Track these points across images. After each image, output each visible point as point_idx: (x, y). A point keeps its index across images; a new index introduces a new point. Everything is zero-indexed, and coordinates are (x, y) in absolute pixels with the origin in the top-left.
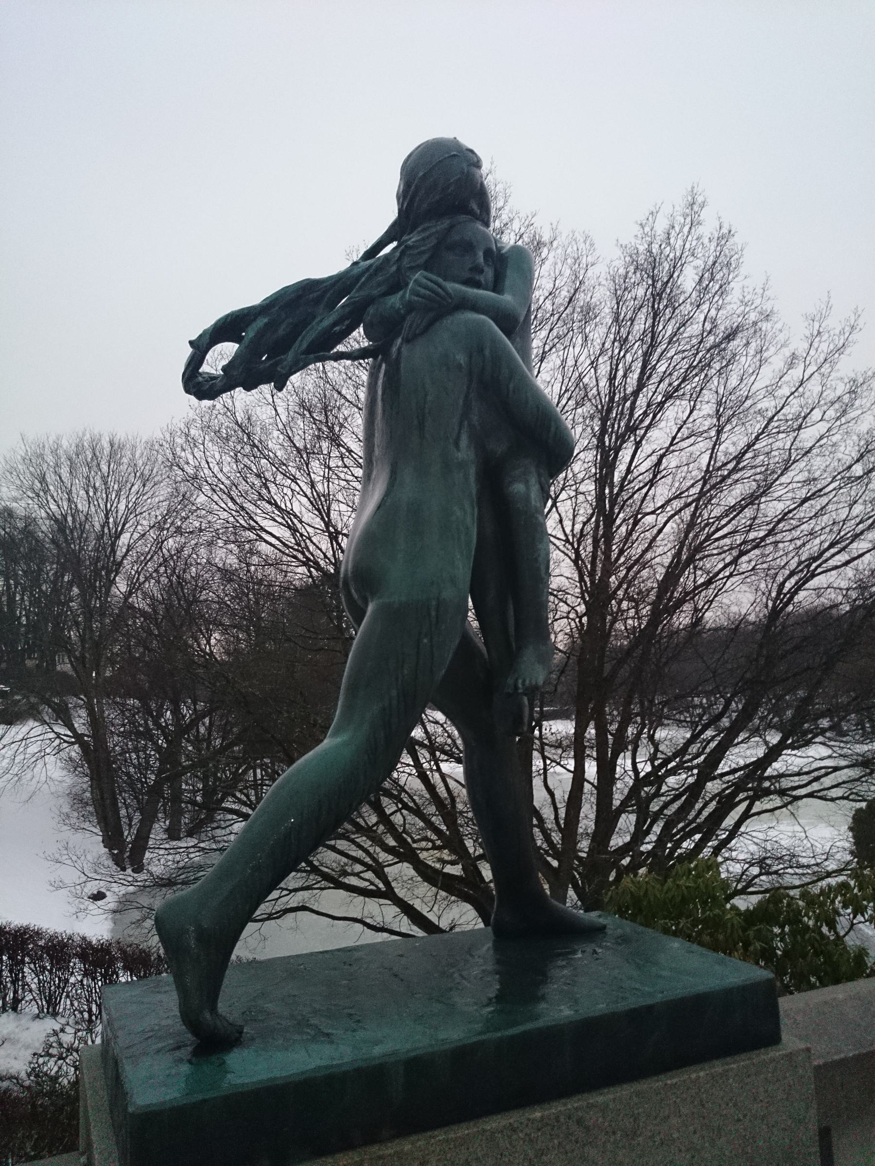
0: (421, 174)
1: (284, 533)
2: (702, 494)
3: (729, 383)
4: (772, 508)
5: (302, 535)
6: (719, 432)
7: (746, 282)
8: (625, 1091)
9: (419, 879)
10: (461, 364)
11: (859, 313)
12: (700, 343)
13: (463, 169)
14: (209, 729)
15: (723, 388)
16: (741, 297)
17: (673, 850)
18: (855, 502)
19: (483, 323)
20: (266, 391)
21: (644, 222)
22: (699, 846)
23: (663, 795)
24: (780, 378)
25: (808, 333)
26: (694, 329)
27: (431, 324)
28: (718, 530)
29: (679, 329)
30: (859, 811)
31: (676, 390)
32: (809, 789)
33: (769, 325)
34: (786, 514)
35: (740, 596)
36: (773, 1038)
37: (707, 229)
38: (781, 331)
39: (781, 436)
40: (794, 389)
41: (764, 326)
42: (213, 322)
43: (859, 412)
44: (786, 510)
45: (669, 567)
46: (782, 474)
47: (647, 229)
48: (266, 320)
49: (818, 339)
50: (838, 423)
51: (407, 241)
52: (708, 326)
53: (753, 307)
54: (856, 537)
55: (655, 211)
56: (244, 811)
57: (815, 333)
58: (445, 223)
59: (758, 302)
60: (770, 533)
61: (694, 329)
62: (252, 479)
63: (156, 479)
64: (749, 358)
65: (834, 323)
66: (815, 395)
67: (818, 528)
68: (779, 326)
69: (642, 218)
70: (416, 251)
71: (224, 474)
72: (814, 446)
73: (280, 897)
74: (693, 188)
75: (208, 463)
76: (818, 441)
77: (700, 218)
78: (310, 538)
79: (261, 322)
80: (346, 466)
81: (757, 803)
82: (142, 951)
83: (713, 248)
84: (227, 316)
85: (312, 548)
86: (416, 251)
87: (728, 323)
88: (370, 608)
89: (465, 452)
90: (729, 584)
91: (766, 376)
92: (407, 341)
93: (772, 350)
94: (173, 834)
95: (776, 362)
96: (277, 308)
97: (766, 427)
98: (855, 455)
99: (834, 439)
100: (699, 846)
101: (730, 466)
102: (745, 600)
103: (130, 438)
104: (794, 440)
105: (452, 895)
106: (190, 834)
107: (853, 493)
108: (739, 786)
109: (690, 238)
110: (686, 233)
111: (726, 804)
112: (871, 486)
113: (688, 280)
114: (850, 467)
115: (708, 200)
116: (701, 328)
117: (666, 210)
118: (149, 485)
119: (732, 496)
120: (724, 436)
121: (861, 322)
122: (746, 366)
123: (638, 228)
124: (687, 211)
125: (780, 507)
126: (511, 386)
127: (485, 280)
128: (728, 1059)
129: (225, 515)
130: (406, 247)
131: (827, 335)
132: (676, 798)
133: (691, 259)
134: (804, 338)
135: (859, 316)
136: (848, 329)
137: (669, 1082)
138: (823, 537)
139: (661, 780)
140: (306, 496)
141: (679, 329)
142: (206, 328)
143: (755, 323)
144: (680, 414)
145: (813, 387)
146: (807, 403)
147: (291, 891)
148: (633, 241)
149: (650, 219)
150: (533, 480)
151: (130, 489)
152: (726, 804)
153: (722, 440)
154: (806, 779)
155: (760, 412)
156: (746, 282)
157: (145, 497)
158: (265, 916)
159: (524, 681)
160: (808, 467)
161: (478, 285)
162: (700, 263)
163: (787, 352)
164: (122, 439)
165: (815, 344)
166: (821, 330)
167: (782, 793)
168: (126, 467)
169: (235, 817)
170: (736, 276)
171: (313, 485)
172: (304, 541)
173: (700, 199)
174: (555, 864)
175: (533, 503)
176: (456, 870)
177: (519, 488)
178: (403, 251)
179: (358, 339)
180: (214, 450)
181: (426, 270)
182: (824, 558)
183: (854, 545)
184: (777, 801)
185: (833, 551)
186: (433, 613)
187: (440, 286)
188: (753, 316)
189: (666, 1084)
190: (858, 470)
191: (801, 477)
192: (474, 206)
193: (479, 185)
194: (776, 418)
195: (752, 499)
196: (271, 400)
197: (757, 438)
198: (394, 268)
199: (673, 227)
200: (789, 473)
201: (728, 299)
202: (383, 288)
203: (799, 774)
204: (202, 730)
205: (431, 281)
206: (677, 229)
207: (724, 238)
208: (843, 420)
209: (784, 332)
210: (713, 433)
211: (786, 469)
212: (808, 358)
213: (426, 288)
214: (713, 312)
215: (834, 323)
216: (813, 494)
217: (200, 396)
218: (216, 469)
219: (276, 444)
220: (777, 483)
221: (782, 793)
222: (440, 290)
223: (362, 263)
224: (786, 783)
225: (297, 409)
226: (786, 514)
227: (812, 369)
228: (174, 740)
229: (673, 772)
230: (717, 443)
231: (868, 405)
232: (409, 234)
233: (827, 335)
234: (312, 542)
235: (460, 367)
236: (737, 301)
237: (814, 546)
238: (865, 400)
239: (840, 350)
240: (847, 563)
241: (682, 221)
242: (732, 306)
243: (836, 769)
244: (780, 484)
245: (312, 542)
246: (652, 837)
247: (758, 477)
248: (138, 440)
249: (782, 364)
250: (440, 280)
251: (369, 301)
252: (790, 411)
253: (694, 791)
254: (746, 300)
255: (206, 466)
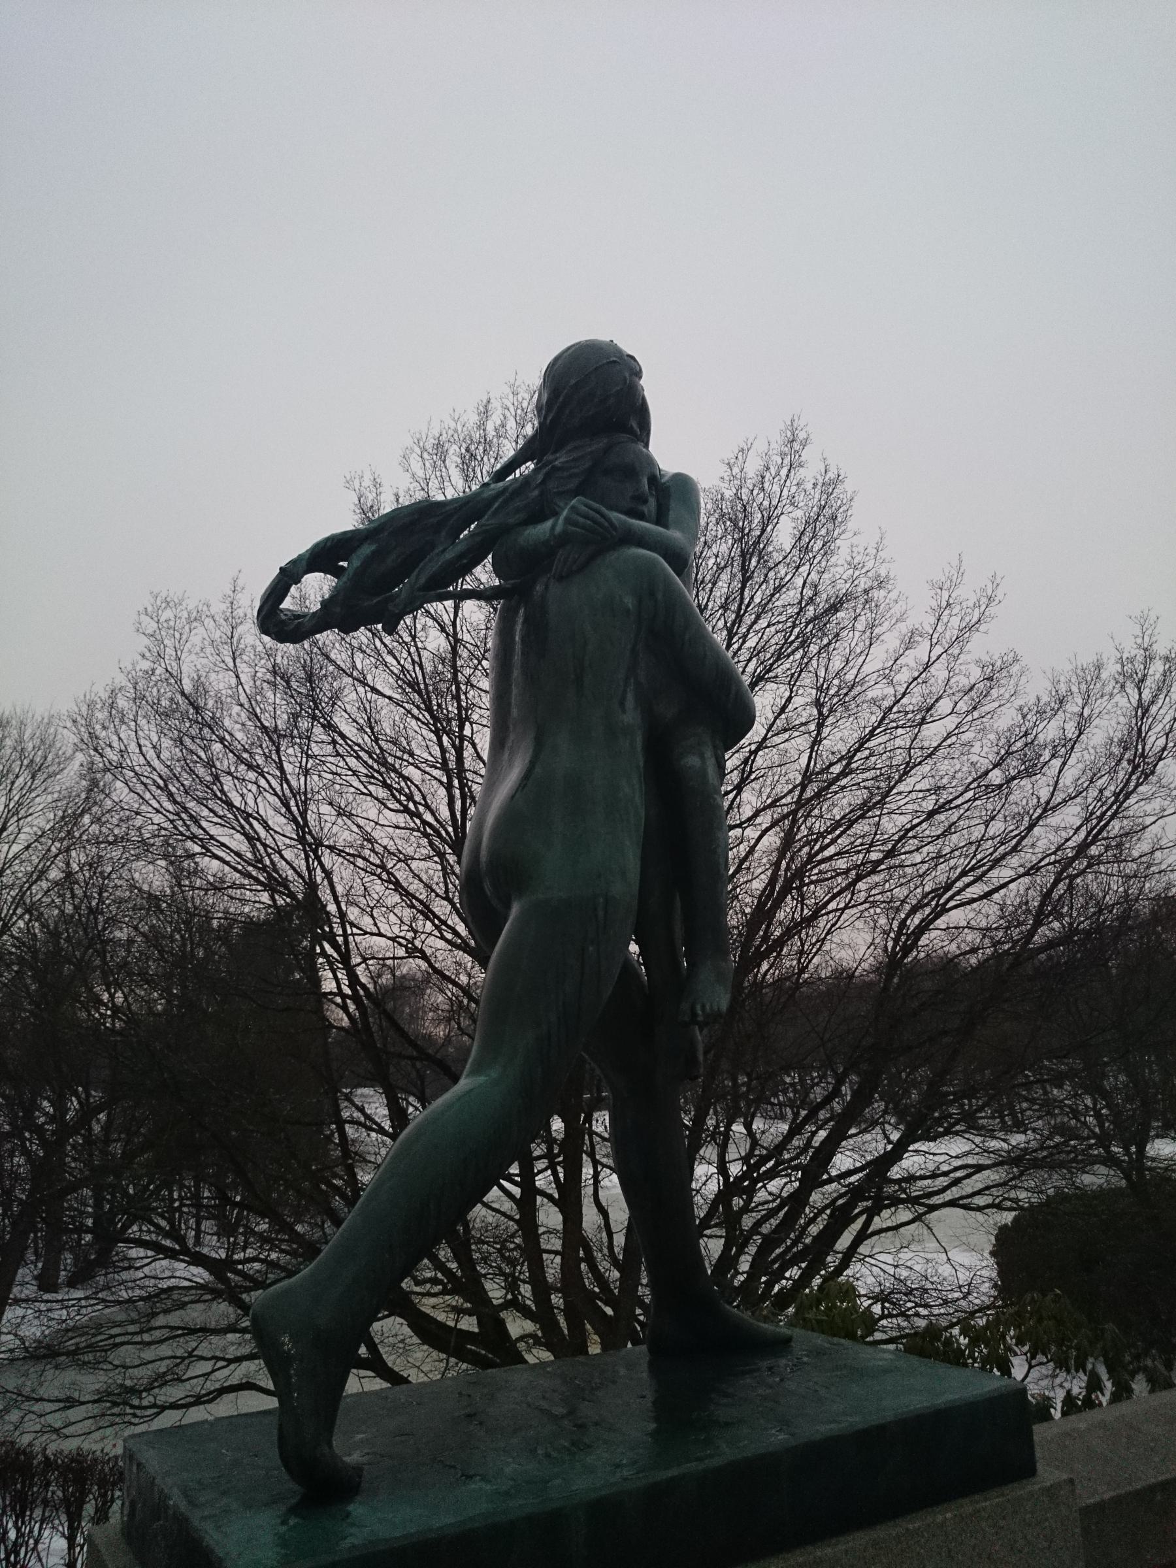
0: (573, 382)
1: (238, 842)
2: (800, 804)
3: (831, 665)
4: (891, 825)
5: (265, 846)
6: (820, 726)
7: (855, 540)
8: (859, 1540)
9: (416, 1340)
10: (629, 610)
11: (998, 581)
12: (798, 614)
13: (625, 377)
14: (107, 1128)
15: (823, 670)
16: (849, 559)
17: (770, 1285)
18: (993, 818)
19: (653, 564)
20: (225, 652)
21: (732, 461)
22: (806, 1278)
23: (752, 1211)
24: (896, 661)
25: (934, 604)
26: (790, 596)
27: (592, 558)
28: (822, 849)
29: (772, 595)
30: (1003, 1231)
31: (769, 671)
32: (948, 1196)
33: (883, 593)
34: (908, 831)
35: (854, 935)
36: (1029, 1470)
37: (809, 473)
38: (896, 602)
39: (900, 731)
40: (916, 674)
41: (875, 594)
42: (309, 546)
43: (996, 704)
44: (909, 826)
45: (761, 896)
46: (900, 781)
47: (736, 470)
48: (373, 547)
49: (947, 612)
50: (969, 718)
51: (550, 462)
52: (808, 592)
53: (864, 571)
54: (996, 863)
55: (746, 448)
56: (168, 1241)
57: (944, 604)
58: (600, 444)
59: (869, 565)
60: (890, 854)
61: (790, 596)
62: (201, 771)
63: (51, 769)
64: (857, 634)
65: (967, 593)
66: (940, 682)
67: (947, 850)
68: (893, 595)
69: (729, 456)
70: (566, 474)
71: (162, 762)
72: (939, 745)
73: (213, 1371)
74: (793, 421)
75: (140, 746)
76: (945, 740)
77: (801, 459)
78: (279, 852)
79: (367, 549)
80: (338, 754)
81: (876, 1219)
82: (19, 1452)
83: (817, 496)
84: (327, 539)
85: (282, 864)
86: (566, 474)
87: (831, 591)
88: (515, 909)
89: (630, 716)
90: (844, 916)
91: (878, 658)
92: (561, 578)
93: (886, 625)
94: (47, 1283)
95: (891, 641)
96: (386, 534)
97: (883, 718)
98: (992, 757)
99: (965, 737)
100: (806, 1278)
101: (837, 769)
102: (860, 941)
103: (18, 710)
104: (915, 739)
105: (463, 1362)
106: (72, 1283)
107: (989, 806)
108: (856, 1193)
109: (788, 482)
110: (784, 478)
111: (840, 1218)
112: (1012, 798)
113: (784, 535)
114: (987, 773)
115: (811, 437)
116: (799, 596)
117: (760, 447)
118: (40, 777)
119: (842, 803)
120: (826, 731)
121: (1000, 593)
122: (853, 645)
123: (726, 468)
124: (786, 449)
125: (902, 820)
126: (687, 637)
127: (649, 511)
128: (977, 1497)
129: (158, 819)
130: (553, 467)
131: (958, 607)
132: (772, 1213)
133: (789, 508)
134: (930, 611)
135: (998, 585)
136: (984, 600)
137: (910, 1527)
138: (952, 862)
139: (751, 1192)
140: (276, 794)
141: (772, 595)
142: (301, 553)
143: (866, 592)
144: (778, 700)
145: (939, 672)
146: (931, 692)
147: (230, 1362)
148: (718, 482)
149: (740, 457)
150: (709, 754)
151: (13, 783)
152: (840, 1218)
153: (823, 735)
154: (942, 1181)
155: (874, 701)
156: (855, 540)
157: (33, 795)
158: (192, 1400)
159: (703, 1007)
160: (933, 773)
161: (641, 517)
162: (799, 513)
163: (903, 628)
164: (7, 713)
165: (945, 619)
166: (951, 601)
167: (914, 1201)
168: (9, 751)
169: (150, 1253)
170: (843, 532)
171: (284, 778)
172: (269, 855)
173: (802, 435)
174: (609, 1311)
175: (711, 781)
176: (469, 1324)
177: (693, 761)
178: (547, 473)
179: (484, 574)
180: (150, 730)
181: (583, 495)
182: (954, 890)
183: (994, 873)
184: (904, 1215)
185: (966, 880)
186: (601, 913)
187: (603, 516)
188: (863, 584)
189: (907, 1529)
190: (996, 777)
191: (925, 785)
192: (634, 424)
193: (640, 401)
194: (895, 710)
195: (864, 810)
196: (231, 665)
197: (872, 734)
198: (536, 493)
199: (768, 469)
200: (908, 780)
201: (833, 560)
202: (521, 516)
203: (934, 1176)
204: (97, 1128)
205: (591, 509)
206: (773, 471)
207: (830, 485)
208: (976, 714)
209: (900, 603)
210: (812, 727)
211: (906, 773)
212: (936, 636)
213: (586, 517)
214: (814, 576)
215: (967, 593)
216: (940, 807)
217: (281, 637)
218: (151, 754)
219: (236, 723)
220: (895, 791)
221: (914, 1201)
222: (602, 520)
223: (493, 486)
224: (917, 1189)
225: (269, 676)
226: (908, 831)
227: (938, 650)
228: (54, 1147)
229: (772, 1175)
230: (817, 742)
231: (1007, 696)
232: (555, 452)
233: (958, 607)
234: (282, 857)
235: (628, 611)
236: (844, 562)
237: (941, 874)
238: (1002, 691)
239: (970, 628)
240: (987, 895)
241: (780, 461)
242: (837, 569)
243: (979, 1168)
244: (899, 793)
245: (282, 857)
246: (744, 1266)
247: (869, 784)
248: (30, 715)
249: (898, 642)
250: (603, 509)
251: (504, 531)
252: (912, 701)
253: (798, 1200)
254: (856, 561)
255: (137, 750)
